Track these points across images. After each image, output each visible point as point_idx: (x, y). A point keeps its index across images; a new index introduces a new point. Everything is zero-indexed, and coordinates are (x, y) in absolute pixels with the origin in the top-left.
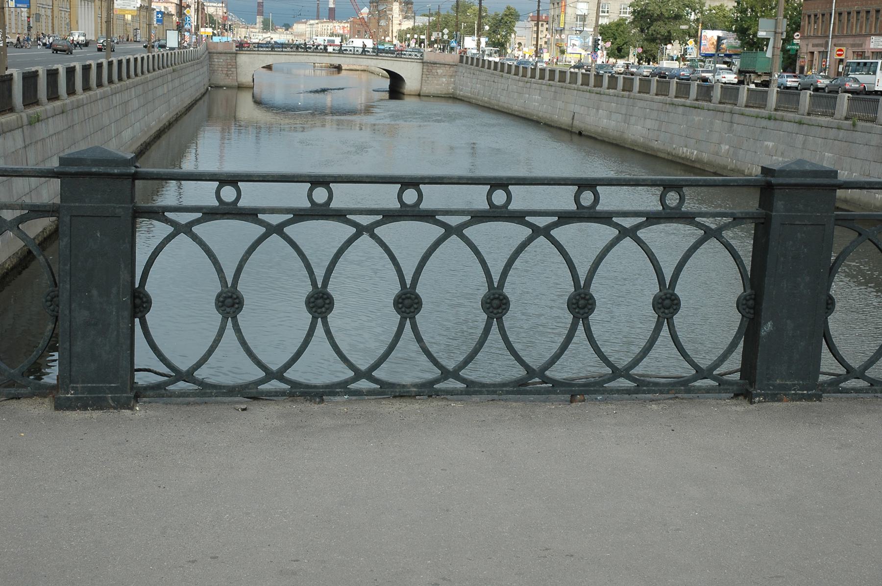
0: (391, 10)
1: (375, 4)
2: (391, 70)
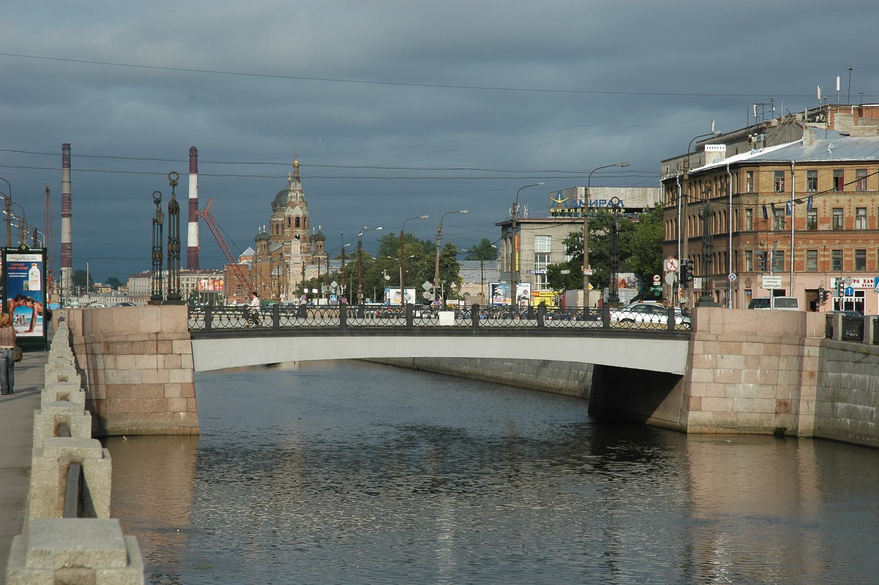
0: (288, 251)
1: (264, 243)
2: (651, 370)
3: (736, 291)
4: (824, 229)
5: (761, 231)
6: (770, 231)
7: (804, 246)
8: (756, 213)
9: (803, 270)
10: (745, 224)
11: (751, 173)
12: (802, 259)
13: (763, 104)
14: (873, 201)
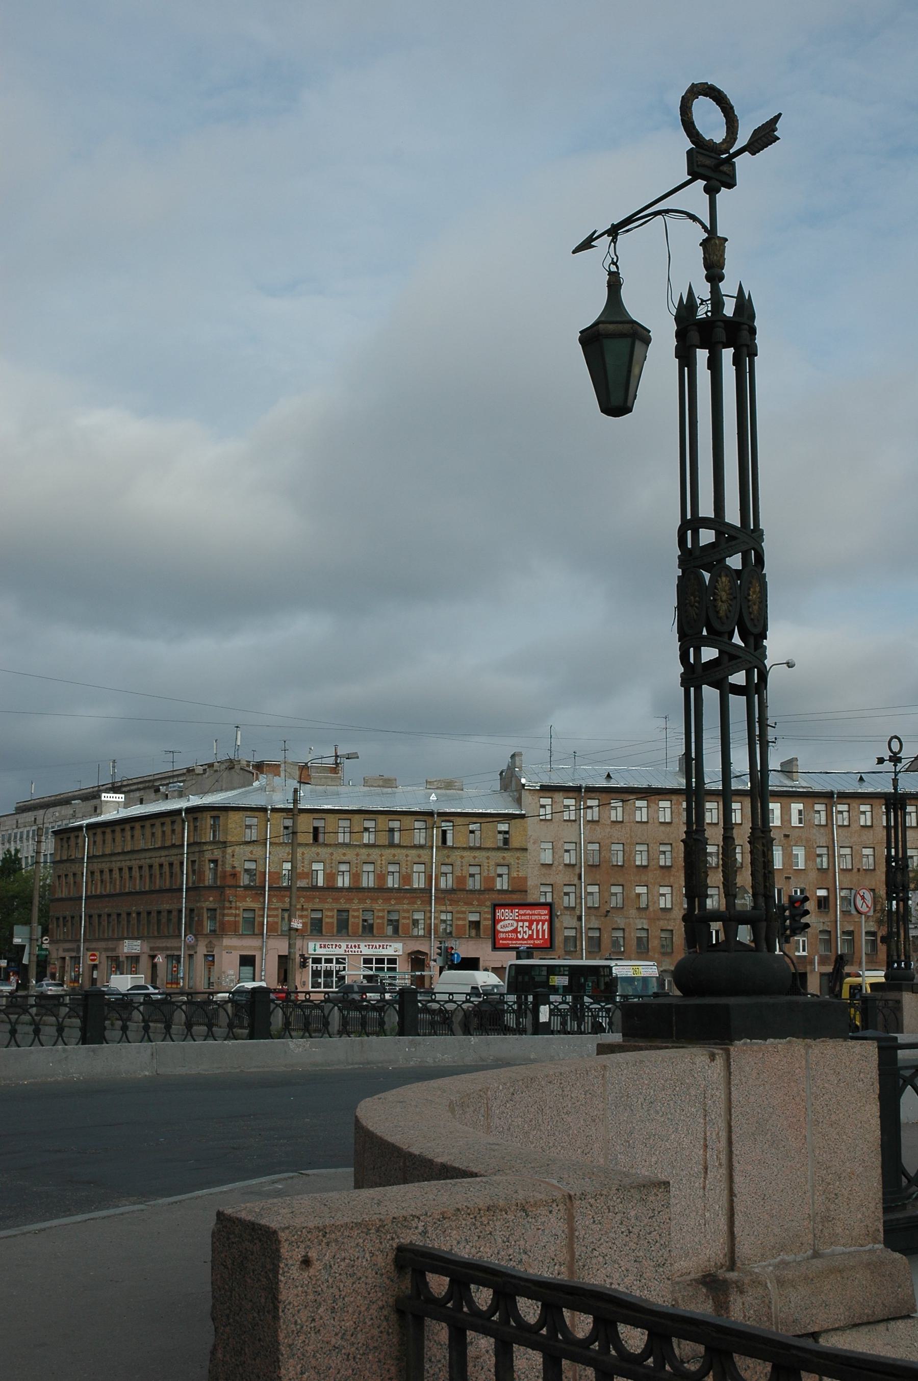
3: (191, 956)
4: (302, 885)
5: (229, 887)
6: (240, 887)
7: (280, 905)
8: (223, 865)
9: (277, 932)
10: (207, 878)
11: (215, 818)
12: (276, 920)
13: (173, 752)
14: (357, 855)
